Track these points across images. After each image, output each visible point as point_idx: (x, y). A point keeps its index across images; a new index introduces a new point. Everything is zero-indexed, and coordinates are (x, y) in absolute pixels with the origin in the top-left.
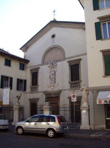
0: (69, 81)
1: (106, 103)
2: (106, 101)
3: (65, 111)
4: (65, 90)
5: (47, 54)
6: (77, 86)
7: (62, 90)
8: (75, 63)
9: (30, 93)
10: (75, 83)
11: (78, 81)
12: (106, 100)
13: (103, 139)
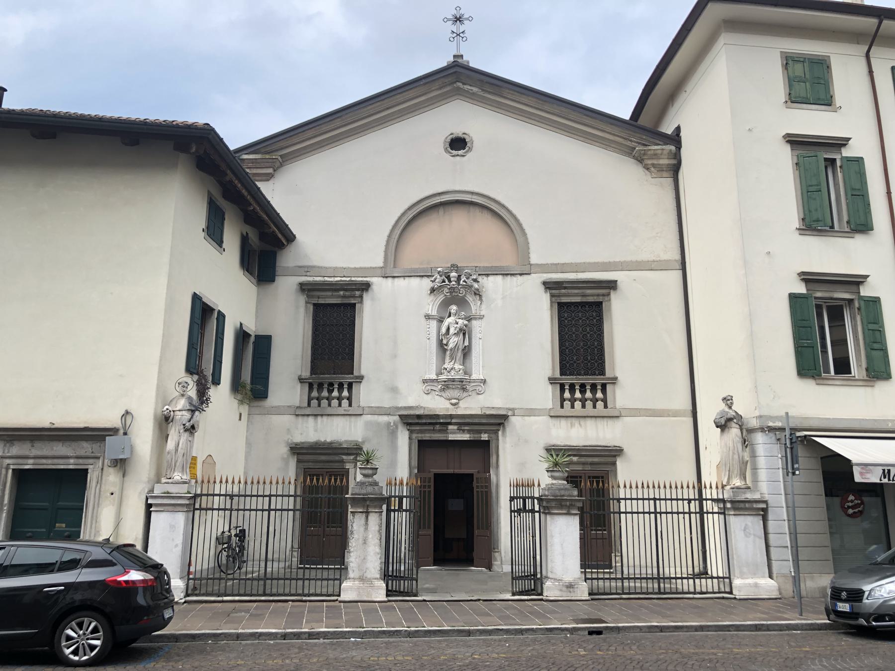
0: (549, 374)
1: (886, 481)
2: (889, 471)
3: (655, 513)
4: (531, 412)
5: (421, 221)
6: (340, 399)
7: (513, 410)
8: (584, 296)
9: (298, 413)
10: (331, 384)
11: (598, 380)
12: (886, 468)
13: (710, 636)
